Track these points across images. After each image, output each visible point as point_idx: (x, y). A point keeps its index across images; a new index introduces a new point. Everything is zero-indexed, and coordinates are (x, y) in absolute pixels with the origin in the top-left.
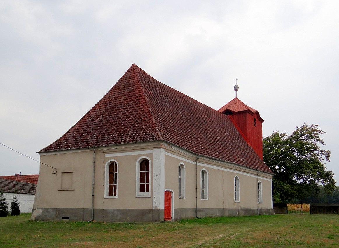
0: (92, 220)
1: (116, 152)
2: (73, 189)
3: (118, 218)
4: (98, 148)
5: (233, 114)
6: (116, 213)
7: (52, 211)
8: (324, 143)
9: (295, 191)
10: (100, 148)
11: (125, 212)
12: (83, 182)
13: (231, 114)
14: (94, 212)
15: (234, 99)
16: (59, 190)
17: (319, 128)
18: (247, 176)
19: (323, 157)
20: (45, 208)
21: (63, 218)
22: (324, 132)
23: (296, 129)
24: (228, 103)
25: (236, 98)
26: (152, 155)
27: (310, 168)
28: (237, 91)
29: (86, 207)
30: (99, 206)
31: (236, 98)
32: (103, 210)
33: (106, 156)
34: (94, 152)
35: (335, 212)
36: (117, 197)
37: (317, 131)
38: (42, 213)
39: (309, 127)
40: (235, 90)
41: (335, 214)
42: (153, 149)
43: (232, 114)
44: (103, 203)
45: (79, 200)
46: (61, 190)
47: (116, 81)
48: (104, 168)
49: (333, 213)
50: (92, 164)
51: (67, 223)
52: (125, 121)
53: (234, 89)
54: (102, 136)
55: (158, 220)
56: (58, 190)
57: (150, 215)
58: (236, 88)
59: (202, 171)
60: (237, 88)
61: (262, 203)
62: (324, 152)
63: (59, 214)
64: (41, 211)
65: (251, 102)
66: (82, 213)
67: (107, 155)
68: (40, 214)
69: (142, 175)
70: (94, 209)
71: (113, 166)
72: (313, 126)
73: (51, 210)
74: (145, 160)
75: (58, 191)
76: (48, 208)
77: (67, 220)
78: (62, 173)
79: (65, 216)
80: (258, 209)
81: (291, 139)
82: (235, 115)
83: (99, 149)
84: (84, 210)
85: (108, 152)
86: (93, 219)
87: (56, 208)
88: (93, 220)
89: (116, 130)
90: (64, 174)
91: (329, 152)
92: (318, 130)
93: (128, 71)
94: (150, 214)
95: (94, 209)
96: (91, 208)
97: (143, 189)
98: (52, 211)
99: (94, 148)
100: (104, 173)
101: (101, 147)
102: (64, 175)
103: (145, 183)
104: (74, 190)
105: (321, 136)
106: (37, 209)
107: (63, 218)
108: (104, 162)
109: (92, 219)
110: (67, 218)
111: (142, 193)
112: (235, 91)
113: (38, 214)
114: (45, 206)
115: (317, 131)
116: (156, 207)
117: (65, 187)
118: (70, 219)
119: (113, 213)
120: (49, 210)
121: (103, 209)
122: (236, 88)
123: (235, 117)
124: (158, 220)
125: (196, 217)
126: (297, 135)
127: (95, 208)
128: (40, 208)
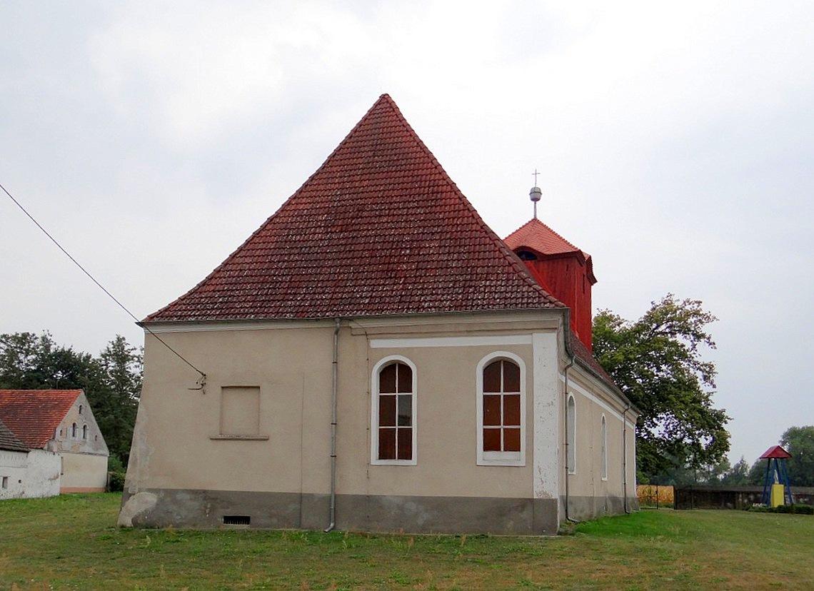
0: (337, 524)
2: (261, 436)
3: (420, 522)
4: (351, 319)
5: (539, 259)
7: (191, 499)
8: (714, 344)
9: (650, 455)
10: (357, 321)
11: (439, 505)
12: (290, 416)
13: (532, 259)
14: (335, 505)
15: (530, 222)
17: (704, 309)
18: (612, 415)
19: (699, 374)
20: (166, 491)
21: (228, 519)
22: (715, 318)
23: (651, 306)
24: (517, 231)
25: (535, 220)
26: (528, 352)
27: (683, 402)
28: (537, 202)
29: (307, 489)
30: (353, 485)
31: (535, 220)
34: (337, 333)
35: (729, 504)
36: (414, 461)
37: (700, 315)
38: (157, 504)
39: (679, 304)
40: (532, 200)
41: (730, 508)
42: (531, 332)
43: (536, 258)
44: (368, 478)
45: (285, 466)
46: (220, 437)
47: (341, 137)
48: (369, 377)
49: (726, 507)
50: (328, 364)
51: (244, 536)
52: (411, 249)
53: (529, 197)
54: (346, 286)
55: (552, 528)
56: (211, 439)
57: (526, 515)
58: (536, 196)
60: (537, 195)
62: (702, 365)
63: (213, 509)
64: (152, 499)
65: (575, 233)
66: (293, 507)
67: (376, 344)
69: (386, 407)
70: (335, 496)
71: (396, 377)
72: (688, 302)
73: (188, 497)
74: (500, 361)
75: (211, 441)
76: (175, 491)
77: (245, 527)
78: (223, 388)
79: (236, 515)
80: (625, 499)
81: (640, 328)
82: (543, 261)
83: (352, 325)
85: (381, 335)
86: (335, 523)
87: (205, 492)
88: (334, 526)
89: (390, 272)
90: (225, 391)
91: (711, 367)
92: (701, 313)
93: (371, 112)
94: (525, 512)
95: (335, 496)
98: (191, 499)
99: (338, 320)
100: (369, 393)
101: (360, 318)
102: (232, 395)
103: (500, 424)
104: (267, 439)
105: (705, 329)
106: (139, 492)
107: (228, 519)
108: (370, 362)
109: (332, 525)
110: (246, 520)
111: (492, 455)
112: (533, 202)
113: (143, 509)
114: (164, 483)
115: (700, 315)
116: (545, 493)
117: (231, 430)
119: (401, 508)
120: (179, 497)
122: (536, 196)
123: (543, 266)
124: (552, 528)
126: (655, 317)
128: (150, 490)
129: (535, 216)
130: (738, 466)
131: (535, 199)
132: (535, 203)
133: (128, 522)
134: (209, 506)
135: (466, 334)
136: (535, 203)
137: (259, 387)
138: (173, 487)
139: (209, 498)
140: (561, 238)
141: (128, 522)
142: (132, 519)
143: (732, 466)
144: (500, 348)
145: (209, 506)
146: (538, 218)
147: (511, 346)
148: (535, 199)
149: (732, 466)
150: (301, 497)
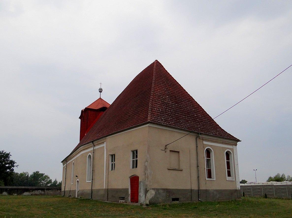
1: (212, 141)
4: (201, 134)
6: (215, 192)
7: (163, 192)
16: (180, 172)
25: (100, 98)
28: (101, 93)
31: (100, 98)
32: (206, 190)
33: (204, 143)
36: (207, 179)
56: (168, 169)
57: (236, 194)
59: (226, 153)
61: (215, 179)
64: (153, 192)
67: (205, 143)
68: (153, 195)
77: (178, 202)
80: (108, 189)
84: (192, 190)
87: (167, 189)
95: (191, 189)
96: (190, 189)
97: (229, 175)
106: (150, 190)
118: (179, 200)
120: (160, 191)
121: (206, 190)
125: (199, 200)
127: (200, 189)
129: (100, 97)
130: (54, 182)
131: (101, 92)
132: (100, 93)
133: (148, 203)
134: (168, 195)
135: (222, 143)
136: (100, 93)
137: (178, 152)
138: (158, 188)
139: (168, 191)
140: (93, 103)
141: (148, 203)
142: (149, 201)
143: (53, 182)
144: (228, 148)
145: (168, 195)
146: (101, 98)
147: (230, 148)
148: (101, 92)
149: (53, 182)
150: (108, 190)
